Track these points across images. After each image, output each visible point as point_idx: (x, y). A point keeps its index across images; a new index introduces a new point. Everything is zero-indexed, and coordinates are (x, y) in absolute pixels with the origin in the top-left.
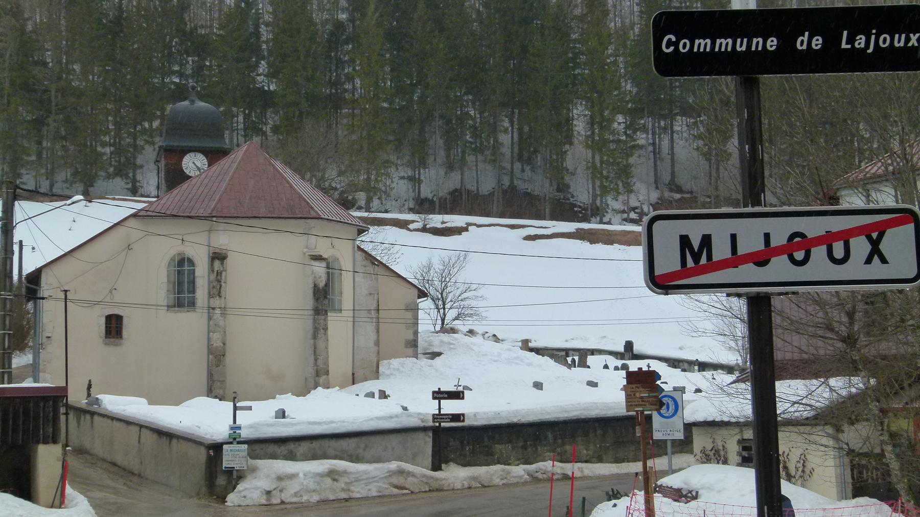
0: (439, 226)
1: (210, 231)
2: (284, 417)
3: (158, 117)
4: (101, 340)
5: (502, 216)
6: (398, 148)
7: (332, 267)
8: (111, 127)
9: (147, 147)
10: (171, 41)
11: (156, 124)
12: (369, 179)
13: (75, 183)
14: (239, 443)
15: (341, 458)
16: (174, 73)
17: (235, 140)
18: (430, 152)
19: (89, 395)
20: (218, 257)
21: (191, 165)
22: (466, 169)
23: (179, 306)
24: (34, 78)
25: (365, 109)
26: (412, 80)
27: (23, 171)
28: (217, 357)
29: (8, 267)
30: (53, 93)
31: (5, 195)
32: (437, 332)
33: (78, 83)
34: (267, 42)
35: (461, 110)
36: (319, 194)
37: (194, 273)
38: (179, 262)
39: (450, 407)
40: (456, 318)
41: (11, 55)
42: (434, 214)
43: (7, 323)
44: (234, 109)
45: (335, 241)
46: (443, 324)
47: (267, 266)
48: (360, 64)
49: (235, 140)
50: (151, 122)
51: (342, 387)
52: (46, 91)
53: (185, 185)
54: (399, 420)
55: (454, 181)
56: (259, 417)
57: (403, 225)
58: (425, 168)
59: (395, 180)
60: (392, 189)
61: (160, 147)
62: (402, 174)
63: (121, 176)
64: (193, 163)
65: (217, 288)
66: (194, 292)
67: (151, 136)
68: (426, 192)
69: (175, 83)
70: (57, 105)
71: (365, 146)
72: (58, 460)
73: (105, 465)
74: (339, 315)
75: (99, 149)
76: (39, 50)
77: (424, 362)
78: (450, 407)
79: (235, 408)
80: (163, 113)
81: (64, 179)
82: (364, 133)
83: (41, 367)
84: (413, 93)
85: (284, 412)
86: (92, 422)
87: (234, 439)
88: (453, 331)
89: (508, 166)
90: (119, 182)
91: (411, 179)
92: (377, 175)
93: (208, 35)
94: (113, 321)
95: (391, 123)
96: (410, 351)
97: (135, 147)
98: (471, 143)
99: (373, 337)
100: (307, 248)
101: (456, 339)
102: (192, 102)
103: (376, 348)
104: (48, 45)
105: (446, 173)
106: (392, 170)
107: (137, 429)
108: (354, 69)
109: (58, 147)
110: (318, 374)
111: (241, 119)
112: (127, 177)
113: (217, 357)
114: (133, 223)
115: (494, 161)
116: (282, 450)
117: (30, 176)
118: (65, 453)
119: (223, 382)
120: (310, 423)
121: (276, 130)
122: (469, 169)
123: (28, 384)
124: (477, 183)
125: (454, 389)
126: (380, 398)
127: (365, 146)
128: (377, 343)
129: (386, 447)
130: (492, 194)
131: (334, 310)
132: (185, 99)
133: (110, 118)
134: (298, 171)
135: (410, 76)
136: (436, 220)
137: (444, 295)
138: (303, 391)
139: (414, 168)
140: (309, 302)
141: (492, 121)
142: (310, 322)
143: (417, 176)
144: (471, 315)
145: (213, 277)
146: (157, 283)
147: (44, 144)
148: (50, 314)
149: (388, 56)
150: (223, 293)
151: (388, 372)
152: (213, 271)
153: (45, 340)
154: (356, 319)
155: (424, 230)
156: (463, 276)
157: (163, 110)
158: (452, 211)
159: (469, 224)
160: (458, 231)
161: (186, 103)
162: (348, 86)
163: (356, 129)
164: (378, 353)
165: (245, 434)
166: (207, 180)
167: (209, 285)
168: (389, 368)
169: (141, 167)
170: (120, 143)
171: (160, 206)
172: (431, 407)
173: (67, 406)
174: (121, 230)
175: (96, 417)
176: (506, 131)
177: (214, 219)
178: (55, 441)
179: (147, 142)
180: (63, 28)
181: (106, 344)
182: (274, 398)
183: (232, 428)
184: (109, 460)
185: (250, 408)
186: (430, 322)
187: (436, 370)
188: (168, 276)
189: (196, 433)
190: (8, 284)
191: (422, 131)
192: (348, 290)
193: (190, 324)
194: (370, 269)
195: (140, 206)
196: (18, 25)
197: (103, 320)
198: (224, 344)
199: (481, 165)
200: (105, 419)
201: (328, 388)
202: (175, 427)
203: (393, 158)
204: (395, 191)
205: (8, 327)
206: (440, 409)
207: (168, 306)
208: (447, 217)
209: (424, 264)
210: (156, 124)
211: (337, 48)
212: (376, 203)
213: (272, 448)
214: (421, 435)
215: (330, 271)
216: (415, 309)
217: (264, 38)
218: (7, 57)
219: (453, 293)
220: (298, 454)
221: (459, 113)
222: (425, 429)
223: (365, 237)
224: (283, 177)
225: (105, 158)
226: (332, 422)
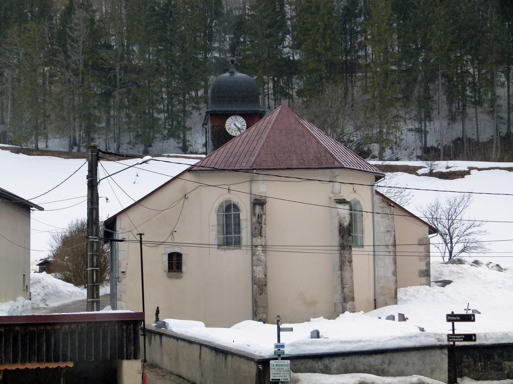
0: (444, 170)
1: (251, 181)
2: (318, 337)
3: (202, 86)
4: (165, 274)
5: (501, 160)
6: (405, 106)
7: (354, 208)
8: (165, 96)
9: (194, 112)
10: (211, 22)
11: (201, 93)
12: (381, 132)
13: (137, 144)
14: (283, 359)
15: (369, 372)
16: (215, 49)
17: (267, 103)
18: (435, 106)
19: (157, 319)
20: (259, 203)
21: (233, 126)
22: (467, 120)
23: (227, 245)
24: (102, 59)
25: (376, 72)
26: (417, 45)
27: (96, 136)
28: (260, 286)
29: (94, 217)
30: (118, 70)
31: (90, 158)
32: (446, 263)
33: (137, 62)
34: (290, 19)
35: (461, 69)
36: (341, 147)
37: (239, 217)
38: (226, 208)
39: (462, 328)
40: (462, 251)
41: (84, 41)
42: (440, 160)
43: (95, 261)
44: (265, 77)
45: (356, 187)
46: (451, 256)
47: (299, 209)
48: (372, 34)
49: (267, 103)
50: (197, 92)
51: (366, 311)
52: (110, 69)
53: (229, 144)
54: (418, 339)
55: (456, 131)
56: (298, 338)
57: (412, 170)
58: (430, 120)
59: (404, 132)
60: (402, 140)
61: (207, 113)
62: (410, 127)
63: (174, 137)
64: (234, 125)
65: (258, 230)
66: (239, 233)
67: (197, 103)
68: (431, 142)
69: (216, 58)
70: (120, 80)
71: (378, 104)
72: (139, 373)
73: (173, 377)
74: (361, 249)
75: (155, 115)
76: (106, 35)
77: (436, 289)
78: (463, 328)
79: (279, 330)
80: (206, 83)
81: (128, 140)
82: (376, 93)
83: (118, 296)
84: (418, 55)
85: (318, 333)
86: (161, 342)
87: (279, 356)
88: (460, 262)
89: (505, 116)
90: (172, 142)
91: (419, 131)
92: (388, 128)
93: (241, 16)
94: (175, 258)
95: (399, 83)
96: (424, 280)
97: (184, 111)
98: (471, 97)
99: (391, 268)
100: (333, 193)
101: (464, 269)
102: (232, 73)
103: (394, 278)
104: (111, 32)
105: (449, 124)
106: (401, 124)
107: (197, 347)
108: (366, 38)
109: (123, 115)
110: (345, 300)
111: (271, 85)
112: (178, 137)
113: (260, 286)
114: (188, 176)
115: (492, 112)
116: (319, 364)
117: (101, 140)
118: (144, 367)
119: (266, 307)
120: (342, 342)
121: (300, 93)
122: (470, 120)
123: (107, 310)
124: (478, 132)
125: (464, 313)
126: (399, 320)
127: (378, 104)
128: (395, 273)
129: (408, 363)
130: (491, 141)
131: (358, 246)
132: (225, 71)
133: (164, 89)
134: (321, 127)
135: (415, 42)
136: (441, 166)
137: (451, 230)
138: (333, 314)
139: (420, 121)
140: (336, 240)
141: (489, 77)
142: (336, 257)
143: (423, 128)
144: (475, 248)
145: (255, 219)
146: (209, 227)
147: (112, 113)
148: (126, 254)
149: (395, 25)
150: (263, 233)
151: (405, 298)
152: (255, 215)
153: (120, 274)
154: (376, 253)
155: (431, 174)
156: (467, 214)
157: (206, 80)
158: (456, 157)
159: (473, 168)
160: (461, 174)
161: (227, 75)
162: (361, 53)
163: (369, 89)
164: (396, 281)
165: (288, 351)
166: (247, 139)
167: (252, 226)
168: (406, 295)
169: (190, 129)
170: (172, 110)
171: (209, 162)
172: (446, 328)
173: (144, 329)
174: (179, 182)
175: (164, 338)
176: (503, 85)
177: (255, 171)
178: (136, 358)
179: (194, 108)
180: (124, 17)
181: (169, 277)
182: (309, 321)
183: (276, 346)
184: (176, 373)
185: (291, 330)
186: (440, 254)
187: (448, 296)
188: (218, 220)
189: (247, 351)
190: (94, 230)
191: (427, 89)
192: (368, 228)
193: (237, 260)
194: (387, 210)
195: (193, 162)
196: (89, 17)
197: (166, 258)
198: (266, 276)
199: (481, 116)
200: (172, 340)
201: (354, 312)
202: (229, 346)
203: (402, 113)
204: (404, 141)
205: (95, 264)
206: (453, 330)
207: (218, 245)
208: (451, 163)
209: (433, 204)
210: (201, 93)
211: (351, 20)
212: (388, 153)
213: (310, 363)
214: (438, 352)
215: (353, 212)
216: (426, 244)
217: (288, 16)
218: (81, 43)
219: (458, 229)
220: (333, 368)
221: (459, 71)
222: (441, 347)
223: (381, 183)
224: (311, 134)
225: (160, 123)
226: (360, 341)
